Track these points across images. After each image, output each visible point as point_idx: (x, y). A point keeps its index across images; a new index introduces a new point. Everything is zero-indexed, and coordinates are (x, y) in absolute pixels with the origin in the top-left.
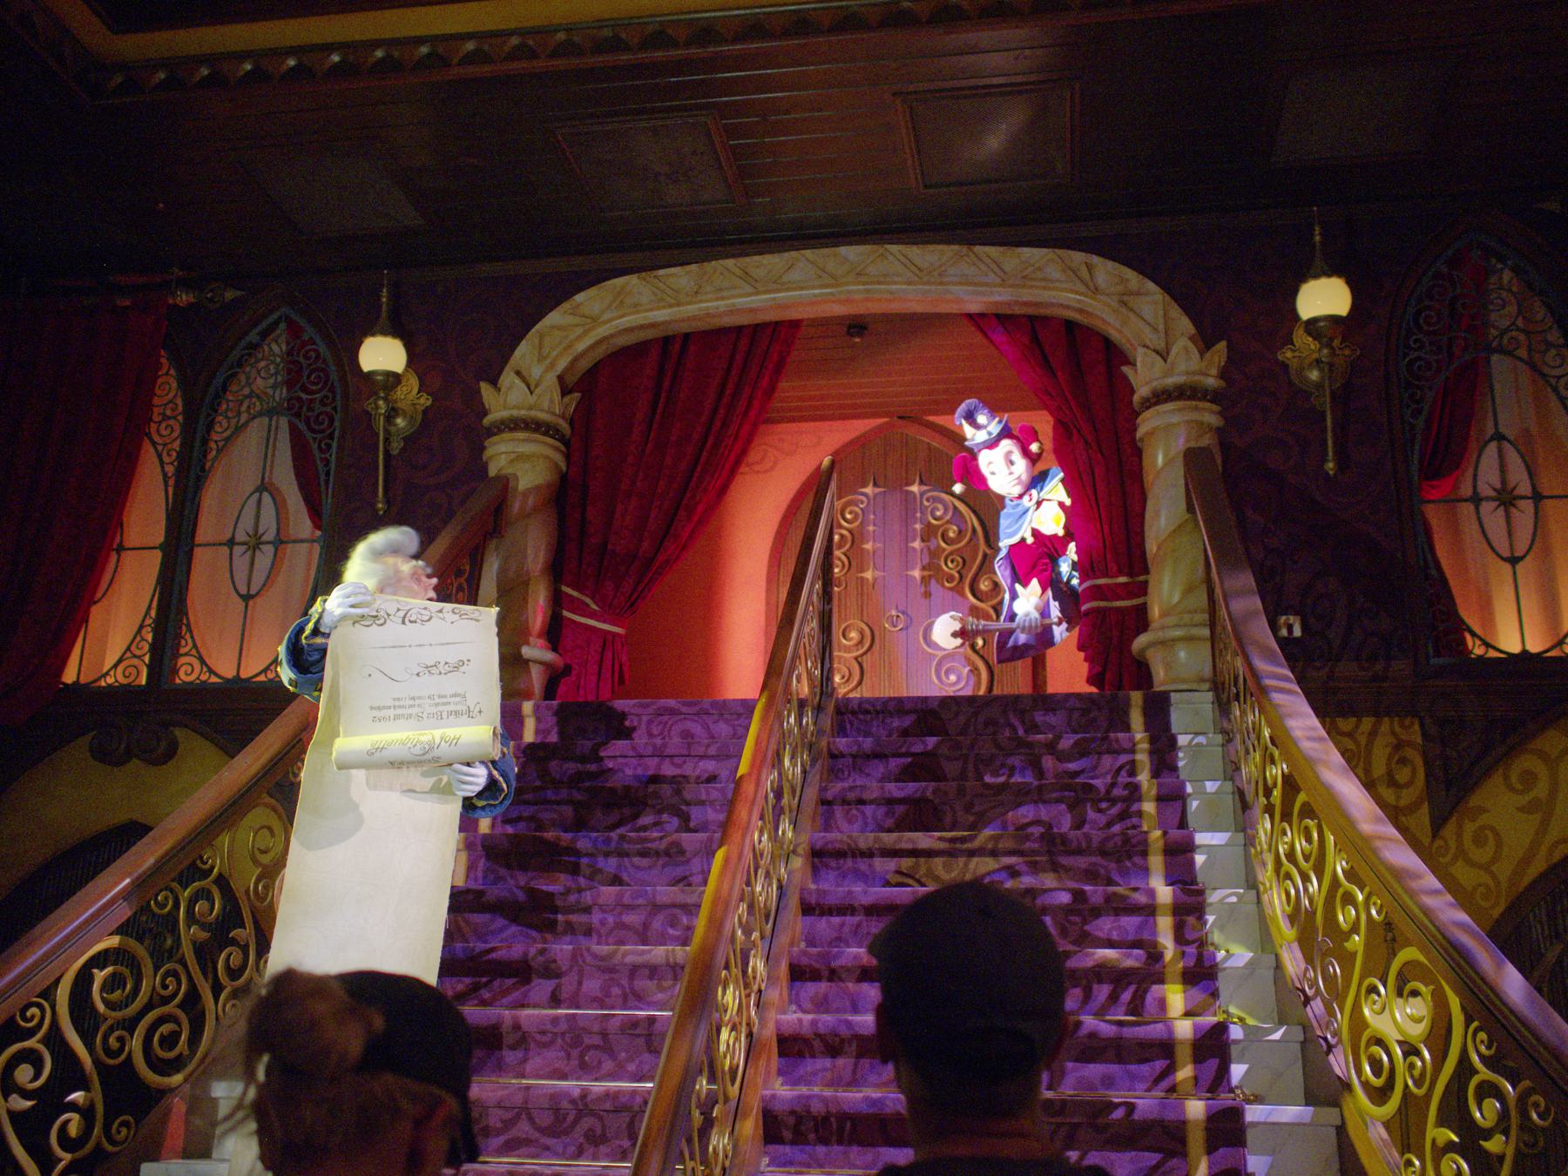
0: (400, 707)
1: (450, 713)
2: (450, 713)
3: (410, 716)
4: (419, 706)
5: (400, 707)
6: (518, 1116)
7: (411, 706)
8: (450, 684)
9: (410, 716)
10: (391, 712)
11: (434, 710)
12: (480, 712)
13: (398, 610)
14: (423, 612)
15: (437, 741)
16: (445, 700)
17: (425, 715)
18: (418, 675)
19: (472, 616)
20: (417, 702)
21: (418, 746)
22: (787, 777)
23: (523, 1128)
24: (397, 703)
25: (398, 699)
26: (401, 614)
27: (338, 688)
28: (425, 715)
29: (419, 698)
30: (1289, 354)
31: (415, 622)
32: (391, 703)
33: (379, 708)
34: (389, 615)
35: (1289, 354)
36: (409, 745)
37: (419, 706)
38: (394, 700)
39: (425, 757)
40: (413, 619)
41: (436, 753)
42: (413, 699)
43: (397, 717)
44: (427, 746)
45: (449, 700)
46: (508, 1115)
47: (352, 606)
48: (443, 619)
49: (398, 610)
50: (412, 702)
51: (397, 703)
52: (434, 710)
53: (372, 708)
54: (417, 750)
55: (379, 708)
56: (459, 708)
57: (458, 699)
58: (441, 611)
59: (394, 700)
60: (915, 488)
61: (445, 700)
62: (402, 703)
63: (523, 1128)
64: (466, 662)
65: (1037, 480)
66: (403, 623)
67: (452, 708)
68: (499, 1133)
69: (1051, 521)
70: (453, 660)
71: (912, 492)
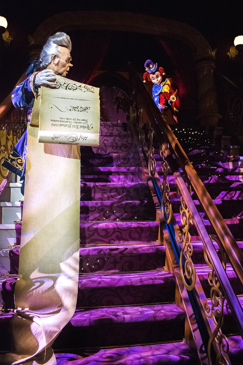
0: (62, 121)
1: (81, 127)
2: (81, 127)
3: (66, 125)
4: (69, 122)
5: (62, 121)
6: (94, 233)
7: (67, 122)
8: (81, 115)
9: (66, 125)
10: (59, 123)
11: (75, 124)
12: (92, 128)
13: (65, 83)
14: (74, 86)
15: (79, 138)
16: (79, 121)
17: (72, 126)
18: (70, 110)
19: (91, 90)
20: (69, 120)
21: (71, 139)
22: (24, 101)
23: (96, 236)
24: (61, 120)
25: (62, 118)
26: (66, 85)
27: (97, 309)
28: (72, 126)
29: (70, 119)
30: (229, 54)
31: (71, 89)
32: (59, 120)
33: (54, 121)
34: (61, 85)
35: (229, 54)
36: (68, 137)
37: (69, 122)
38: (60, 118)
39: (73, 143)
40: (70, 88)
41: (78, 142)
42: (68, 119)
43: (61, 125)
44: (74, 139)
45: (81, 121)
46: (91, 233)
47: (50, 81)
48: (81, 90)
49: (65, 83)
50: (67, 120)
51: (61, 120)
52: (75, 124)
53: (51, 120)
54: (71, 140)
55: (54, 121)
56: (84, 125)
57: (84, 122)
58: (80, 86)
59: (60, 118)
60: (114, 88)
61: (79, 121)
62: (63, 120)
63: (96, 236)
64: (89, 108)
65: (163, 80)
66: (66, 89)
67: (82, 124)
68: (89, 238)
69: (166, 89)
70: (84, 107)
71: (114, 88)
